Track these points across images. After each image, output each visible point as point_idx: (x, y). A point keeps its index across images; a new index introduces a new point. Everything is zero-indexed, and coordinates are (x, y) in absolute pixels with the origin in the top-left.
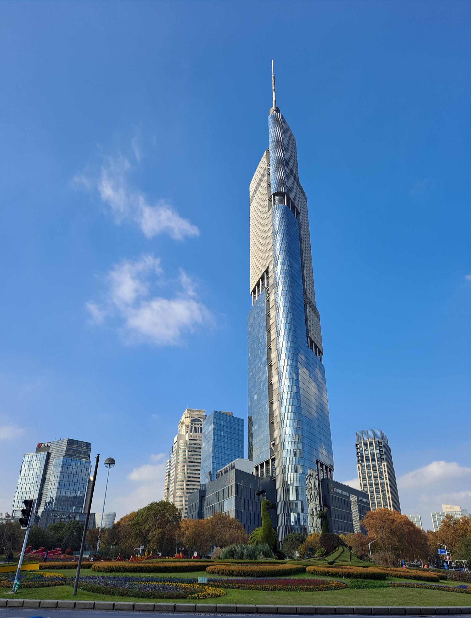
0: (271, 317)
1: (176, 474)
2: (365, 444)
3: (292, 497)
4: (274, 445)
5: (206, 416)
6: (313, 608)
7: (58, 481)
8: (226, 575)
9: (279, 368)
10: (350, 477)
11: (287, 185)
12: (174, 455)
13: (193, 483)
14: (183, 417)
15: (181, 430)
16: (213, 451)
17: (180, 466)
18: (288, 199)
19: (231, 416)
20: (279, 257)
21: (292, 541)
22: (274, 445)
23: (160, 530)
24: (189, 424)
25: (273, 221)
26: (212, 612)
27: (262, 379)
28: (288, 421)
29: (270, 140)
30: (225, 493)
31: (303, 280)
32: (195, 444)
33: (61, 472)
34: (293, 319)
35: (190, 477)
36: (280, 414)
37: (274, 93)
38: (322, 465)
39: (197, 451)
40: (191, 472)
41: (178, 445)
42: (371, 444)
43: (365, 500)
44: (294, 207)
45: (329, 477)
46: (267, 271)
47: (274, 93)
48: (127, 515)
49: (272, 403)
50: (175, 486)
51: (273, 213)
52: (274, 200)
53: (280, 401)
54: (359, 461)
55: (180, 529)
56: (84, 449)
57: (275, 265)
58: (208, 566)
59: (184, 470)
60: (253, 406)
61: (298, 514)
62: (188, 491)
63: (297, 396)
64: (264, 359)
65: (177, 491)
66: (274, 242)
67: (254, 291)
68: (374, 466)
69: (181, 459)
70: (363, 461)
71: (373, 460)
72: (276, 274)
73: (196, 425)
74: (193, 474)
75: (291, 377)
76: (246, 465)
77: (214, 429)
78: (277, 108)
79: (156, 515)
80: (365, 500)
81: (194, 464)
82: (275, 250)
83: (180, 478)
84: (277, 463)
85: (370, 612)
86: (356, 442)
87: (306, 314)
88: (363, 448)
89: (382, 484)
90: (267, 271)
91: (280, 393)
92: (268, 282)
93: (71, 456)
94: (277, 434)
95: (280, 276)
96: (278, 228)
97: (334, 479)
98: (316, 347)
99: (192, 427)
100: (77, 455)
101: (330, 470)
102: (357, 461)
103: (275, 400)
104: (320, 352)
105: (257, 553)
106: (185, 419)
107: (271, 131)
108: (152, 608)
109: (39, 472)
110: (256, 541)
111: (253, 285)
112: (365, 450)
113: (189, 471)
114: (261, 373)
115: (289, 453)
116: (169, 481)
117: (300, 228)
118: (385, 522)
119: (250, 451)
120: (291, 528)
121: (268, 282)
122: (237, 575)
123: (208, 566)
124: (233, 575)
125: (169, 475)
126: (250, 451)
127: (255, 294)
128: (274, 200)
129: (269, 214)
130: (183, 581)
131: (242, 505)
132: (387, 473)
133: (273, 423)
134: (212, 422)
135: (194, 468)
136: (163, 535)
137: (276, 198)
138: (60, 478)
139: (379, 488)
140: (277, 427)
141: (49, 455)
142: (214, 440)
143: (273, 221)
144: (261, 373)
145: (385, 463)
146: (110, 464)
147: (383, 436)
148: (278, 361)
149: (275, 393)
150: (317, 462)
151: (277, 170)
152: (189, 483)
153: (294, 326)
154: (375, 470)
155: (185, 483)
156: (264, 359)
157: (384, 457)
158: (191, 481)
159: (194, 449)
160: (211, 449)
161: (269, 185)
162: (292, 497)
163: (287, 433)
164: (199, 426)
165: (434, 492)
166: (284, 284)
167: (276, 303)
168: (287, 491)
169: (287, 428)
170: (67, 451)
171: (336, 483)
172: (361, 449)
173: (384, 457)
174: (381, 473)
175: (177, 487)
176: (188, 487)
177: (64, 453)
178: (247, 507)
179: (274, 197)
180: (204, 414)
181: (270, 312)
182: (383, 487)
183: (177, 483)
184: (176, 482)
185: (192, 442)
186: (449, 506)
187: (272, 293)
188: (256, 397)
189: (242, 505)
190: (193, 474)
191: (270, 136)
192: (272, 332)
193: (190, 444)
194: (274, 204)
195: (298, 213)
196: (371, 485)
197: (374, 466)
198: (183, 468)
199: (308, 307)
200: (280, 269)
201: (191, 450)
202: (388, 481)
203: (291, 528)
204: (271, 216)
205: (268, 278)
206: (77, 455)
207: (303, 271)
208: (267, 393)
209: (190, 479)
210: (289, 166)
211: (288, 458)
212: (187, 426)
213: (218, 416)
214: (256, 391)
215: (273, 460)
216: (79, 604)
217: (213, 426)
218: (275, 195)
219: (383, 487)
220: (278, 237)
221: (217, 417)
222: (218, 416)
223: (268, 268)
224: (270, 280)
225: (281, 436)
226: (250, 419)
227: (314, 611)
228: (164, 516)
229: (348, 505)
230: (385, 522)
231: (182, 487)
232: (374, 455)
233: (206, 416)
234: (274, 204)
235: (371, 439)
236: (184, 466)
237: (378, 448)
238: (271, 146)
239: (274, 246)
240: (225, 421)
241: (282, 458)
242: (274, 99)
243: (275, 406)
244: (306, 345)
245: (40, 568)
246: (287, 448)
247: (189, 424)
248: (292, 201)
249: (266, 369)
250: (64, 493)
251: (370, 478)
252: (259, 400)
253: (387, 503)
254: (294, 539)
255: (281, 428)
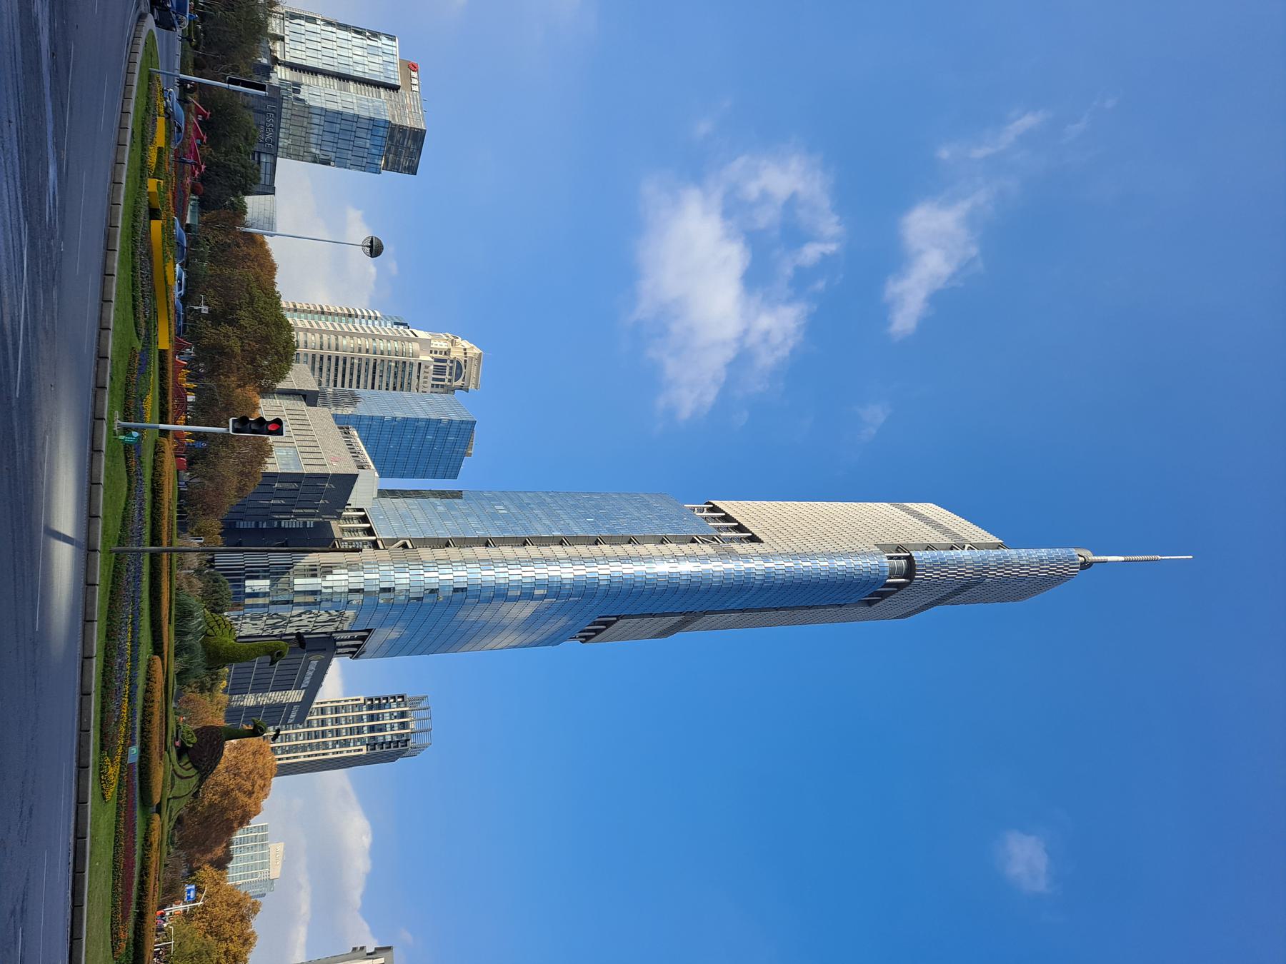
0: (661, 547)
1: (352, 335)
2: (403, 715)
3: (301, 583)
4: (405, 546)
5: (467, 390)
6: (86, 833)
7: (340, 109)
8: (144, 708)
9: (557, 560)
10: (338, 683)
11: (930, 585)
12: (389, 329)
13: (333, 369)
14: (466, 344)
15: (440, 339)
16: (394, 419)
17: (368, 343)
18: (899, 586)
19: (465, 454)
20: (779, 566)
21: (215, 592)
22: (405, 546)
23: (238, 350)
24: (453, 355)
25: (856, 554)
26: (76, 830)
27: (537, 524)
28: (451, 577)
29: (1023, 552)
30: (311, 450)
31: (733, 611)
32: (410, 374)
33: (358, 117)
34: (653, 592)
35: (345, 363)
36: (465, 562)
37: (1122, 558)
38: (363, 638)
39: (396, 377)
40: (356, 366)
41: (410, 340)
42: (404, 725)
43: (293, 716)
44: (883, 595)
45: (340, 650)
46: (754, 539)
47: (1122, 558)
48: (272, 269)
49: (487, 545)
50: (328, 332)
51: (873, 554)
52: (899, 558)
53: (491, 562)
54: (371, 700)
55: (239, 386)
56: (405, 163)
57: (765, 557)
58: (162, 659)
59: (360, 351)
60: (483, 502)
61: (265, 595)
62: (318, 359)
63: (500, 594)
64: (575, 528)
65: (318, 336)
66: (813, 555)
67: (715, 509)
68: (360, 730)
69: (382, 345)
70: (370, 708)
71: (372, 729)
72: (746, 557)
73: (449, 373)
74: (352, 369)
75: (537, 584)
76: (363, 495)
77: (439, 421)
78: (1091, 564)
79: (266, 339)
80: (293, 716)
81: (371, 371)
82: (795, 556)
83: (344, 342)
84: (368, 552)
85: (78, 869)
86: (408, 696)
87: (663, 615)
88: (395, 709)
89: (325, 745)
90: (754, 539)
91: (506, 561)
92: (731, 539)
93: (391, 137)
94: (425, 553)
95: (743, 566)
96: (840, 563)
97: (335, 662)
98: (598, 632)
99: (445, 361)
100: (393, 148)
101: (353, 653)
102: (371, 696)
103: (493, 552)
104: (587, 638)
105: (186, 657)
106: (463, 348)
107: (1043, 552)
108: (85, 728)
109: (360, 68)
110: (210, 631)
111: (727, 506)
112: (391, 714)
113: (356, 361)
114: (547, 522)
115: (387, 579)
116: (338, 314)
117: (841, 606)
118: (248, 778)
119: (393, 493)
120: (239, 580)
121: (731, 539)
122: (143, 730)
123: (162, 659)
124: (143, 722)
125: (350, 316)
126: (393, 493)
127: (710, 510)
128: (899, 558)
129: (869, 546)
130: (135, 633)
131: (287, 485)
132: (345, 754)
133: (448, 545)
134: (454, 418)
135: (363, 371)
136: (230, 355)
137: (903, 562)
138: (348, 115)
139: (316, 737)
140: (440, 553)
141: (395, 88)
142: (417, 420)
143: (856, 554)
144: (547, 522)
145: (364, 752)
146: (371, 247)
147: (417, 750)
148: (571, 559)
149: (507, 551)
150: (369, 631)
151: (960, 564)
152: (333, 360)
153: (641, 593)
154: (351, 731)
155: (333, 353)
156: (575, 528)
157: (378, 750)
158: (337, 364)
159: (399, 374)
160: (399, 415)
161: (929, 547)
162: (301, 583)
163: (427, 575)
164: (447, 376)
165: (309, 848)
166: (726, 576)
167: (687, 557)
168: (313, 572)
169: (436, 574)
170: (401, 127)
171: (328, 665)
172: (394, 705)
173: (378, 750)
174: (346, 743)
175: (325, 337)
176: (325, 360)
177: (397, 121)
178: (284, 494)
179: (905, 558)
180: (472, 387)
181: (670, 545)
182: (318, 746)
183: (333, 337)
184: (336, 334)
185: (415, 369)
186: (280, 857)
187: (707, 549)
188: (501, 509)
189: (287, 485)
190: (352, 369)
191: (1032, 552)
192: (628, 547)
193: (411, 364)
194: (891, 558)
195: (870, 603)
196: (323, 723)
197: (360, 730)
198: (363, 350)
199: (678, 618)
200: (757, 566)
201: (400, 365)
202: (331, 756)
203: (239, 580)
204: (866, 550)
205: (740, 540)
206: (393, 148)
207: (751, 610)
208: (507, 535)
209: (341, 363)
210: (968, 588)
211: (377, 576)
212: (447, 352)
213: (465, 430)
214: (513, 510)
215: (375, 545)
216: (94, 592)
217: (445, 419)
218: (910, 559)
219: (318, 746)
220: (823, 563)
221: (463, 426)
222: (465, 430)
223: (760, 541)
224: (735, 546)
225: (419, 560)
226: (457, 495)
227: (78, 869)
228: (265, 354)
229: (284, 686)
230: (248, 778)
231: (325, 346)
232: (381, 730)
233: (467, 390)
234: (891, 558)
235: (412, 726)
236: (367, 351)
237: (395, 739)
238: (1012, 553)
239: (804, 556)
240: (455, 443)
241: (378, 563)
242: (1110, 558)
243: (480, 551)
244: (599, 614)
245: (163, 354)
246: (397, 575)
247: (453, 355)
248: (894, 592)
249: (556, 534)
250: (316, 131)
251: (337, 721)
252: (494, 516)
253: (288, 752)
254: (217, 596)
255: (436, 562)
